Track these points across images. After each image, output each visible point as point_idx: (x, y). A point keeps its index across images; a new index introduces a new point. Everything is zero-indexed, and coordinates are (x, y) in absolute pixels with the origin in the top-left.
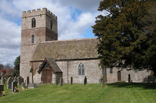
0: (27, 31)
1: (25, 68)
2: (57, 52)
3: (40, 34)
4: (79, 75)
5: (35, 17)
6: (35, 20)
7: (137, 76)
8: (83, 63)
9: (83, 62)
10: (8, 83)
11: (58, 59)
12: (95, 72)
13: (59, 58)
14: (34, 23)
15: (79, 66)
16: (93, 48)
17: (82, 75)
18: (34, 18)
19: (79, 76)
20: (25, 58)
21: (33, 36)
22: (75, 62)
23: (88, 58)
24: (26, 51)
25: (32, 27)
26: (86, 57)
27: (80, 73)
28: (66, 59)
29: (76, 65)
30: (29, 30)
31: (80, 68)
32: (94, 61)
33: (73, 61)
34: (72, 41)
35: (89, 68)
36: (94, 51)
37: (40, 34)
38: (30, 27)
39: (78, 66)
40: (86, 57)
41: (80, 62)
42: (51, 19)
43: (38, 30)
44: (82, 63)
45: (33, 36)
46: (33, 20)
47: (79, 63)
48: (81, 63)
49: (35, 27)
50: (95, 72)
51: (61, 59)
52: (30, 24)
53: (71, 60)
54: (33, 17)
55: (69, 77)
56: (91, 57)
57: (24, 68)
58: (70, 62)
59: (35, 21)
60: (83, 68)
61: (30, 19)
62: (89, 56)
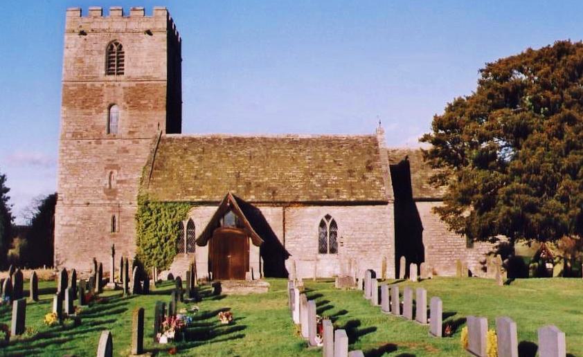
0: (88, 84)
1: (79, 223)
3: (143, 102)
7: (474, 258)
9: (335, 212)
10: (531, 271)
12: (374, 244)
13: (253, 197)
14: (114, 59)
15: (322, 224)
16: (358, 168)
23: (352, 200)
24: (85, 160)
25: (109, 72)
26: (344, 197)
28: (278, 198)
33: (301, 209)
35: (354, 231)
36: (364, 178)
37: (143, 102)
40: (345, 197)
43: (132, 87)
46: (112, 47)
47: (322, 216)
48: (328, 217)
50: (374, 244)
51: (261, 198)
52: (102, 60)
53: (295, 203)
56: (362, 197)
61: (112, 134)
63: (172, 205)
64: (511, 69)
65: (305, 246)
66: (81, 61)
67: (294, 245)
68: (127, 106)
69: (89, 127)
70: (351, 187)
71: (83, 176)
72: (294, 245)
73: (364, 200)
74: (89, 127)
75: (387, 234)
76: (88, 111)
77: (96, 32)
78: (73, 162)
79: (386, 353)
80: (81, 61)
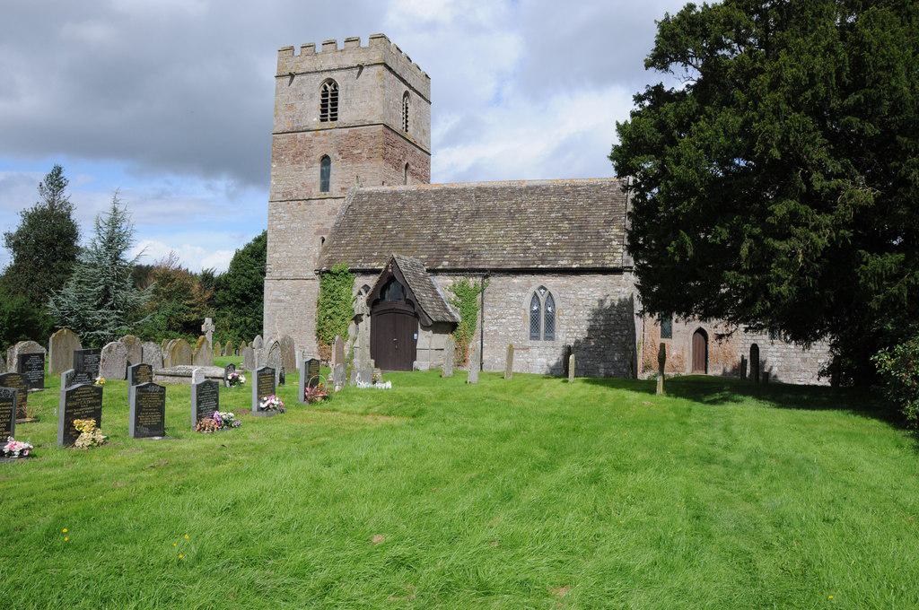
0: (299, 134)
2: (435, 236)
3: (356, 152)
4: (532, 338)
5: (335, 76)
6: (335, 86)
8: (550, 289)
9: (551, 282)
11: (440, 267)
17: (546, 338)
18: (330, 81)
19: (529, 343)
20: (290, 255)
21: (326, 160)
22: (518, 280)
23: (574, 266)
25: (323, 120)
26: (563, 263)
27: (534, 335)
29: (520, 294)
30: (308, 134)
31: (535, 308)
32: (599, 279)
34: (503, 189)
37: (356, 152)
38: (314, 118)
39: (528, 298)
41: (537, 281)
42: (407, 89)
44: (545, 289)
45: (326, 160)
46: (325, 87)
47: (533, 289)
49: (336, 119)
54: (328, 75)
55: (485, 345)
56: (589, 263)
57: (281, 301)
58: (493, 280)
59: (335, 94)
60: (550, 309)
61: (314, 86)
62: (576, 259)
63: (132, 476)
64: (786, 47)
65: (510, 329)
66: (291, 107)
67: (495, 328)
68: (340, 157)
69: (299, 186)
70: (579, 247)
71: (292, 243)
72: (495, 328)
73: (591, 266)
74: (299, 186)
75: (624, 315)
76: (297, 166)
77: (350, 437)
78: (283, 227)
79: (216, 275)
80: (291, 107)
